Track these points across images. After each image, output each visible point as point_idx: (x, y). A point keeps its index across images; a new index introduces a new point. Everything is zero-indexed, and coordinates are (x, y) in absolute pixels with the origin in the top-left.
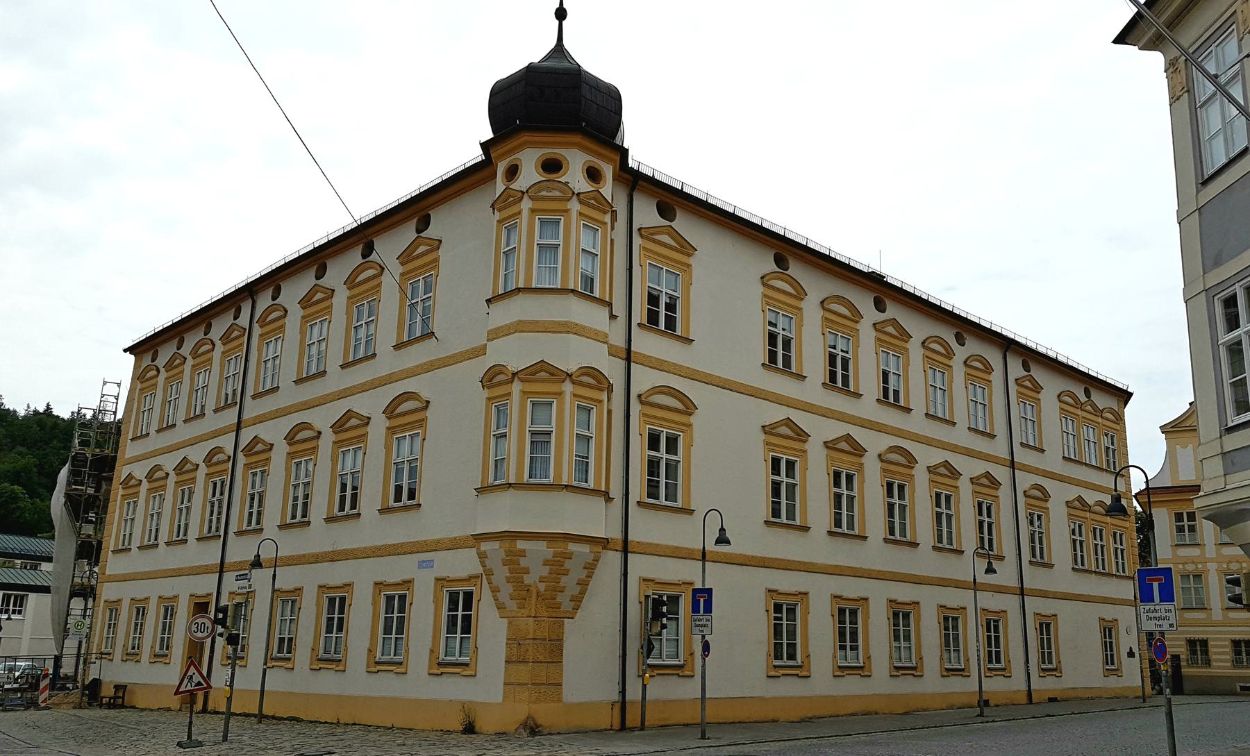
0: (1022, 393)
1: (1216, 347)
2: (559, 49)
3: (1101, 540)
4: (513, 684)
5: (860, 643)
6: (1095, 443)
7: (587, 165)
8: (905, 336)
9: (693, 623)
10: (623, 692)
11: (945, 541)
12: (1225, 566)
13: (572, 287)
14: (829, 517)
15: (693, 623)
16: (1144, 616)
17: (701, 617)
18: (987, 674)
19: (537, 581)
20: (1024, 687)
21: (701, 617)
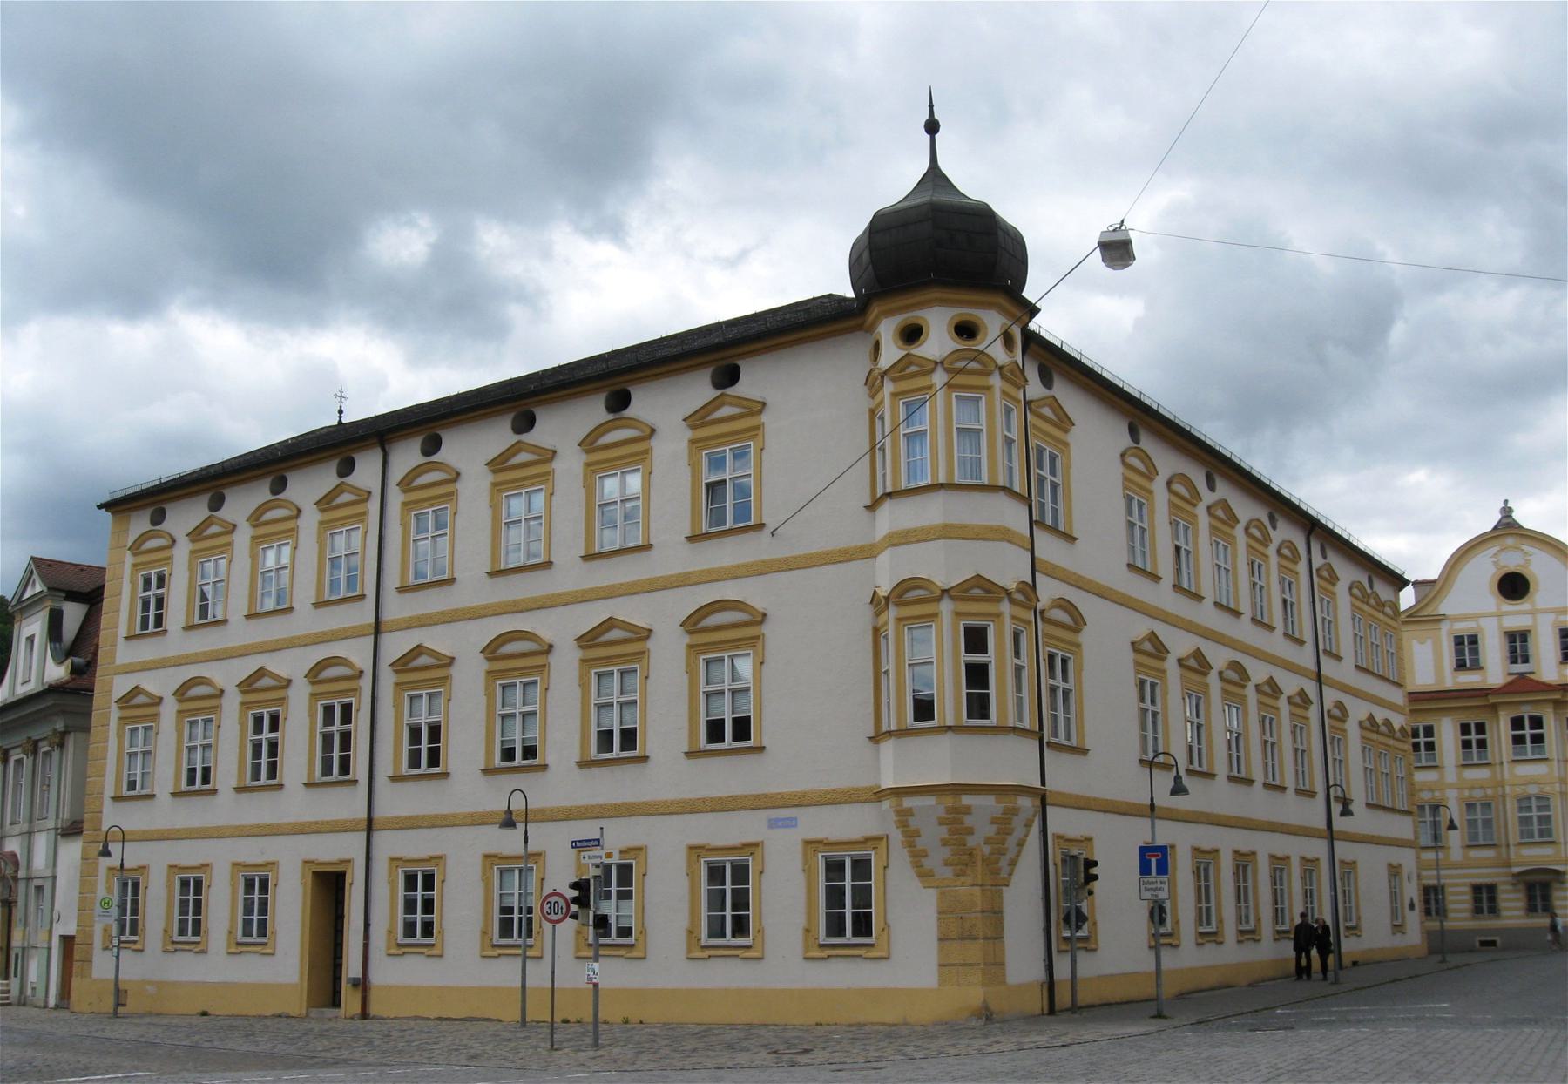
0: (1253, 548)
2: (934, 176)
3: (1065, 679)
4: (953, 965)
5: (497, 916)
6: (1227, 570)
7: (957, 320)
8: (1232, 519)
9: (1143, 887)
11: (1271, 778)
12: (1466, 793)
13: (1001, 484)
15: (1143, 887)
17: (1154, 880)
21: (1154, 880)
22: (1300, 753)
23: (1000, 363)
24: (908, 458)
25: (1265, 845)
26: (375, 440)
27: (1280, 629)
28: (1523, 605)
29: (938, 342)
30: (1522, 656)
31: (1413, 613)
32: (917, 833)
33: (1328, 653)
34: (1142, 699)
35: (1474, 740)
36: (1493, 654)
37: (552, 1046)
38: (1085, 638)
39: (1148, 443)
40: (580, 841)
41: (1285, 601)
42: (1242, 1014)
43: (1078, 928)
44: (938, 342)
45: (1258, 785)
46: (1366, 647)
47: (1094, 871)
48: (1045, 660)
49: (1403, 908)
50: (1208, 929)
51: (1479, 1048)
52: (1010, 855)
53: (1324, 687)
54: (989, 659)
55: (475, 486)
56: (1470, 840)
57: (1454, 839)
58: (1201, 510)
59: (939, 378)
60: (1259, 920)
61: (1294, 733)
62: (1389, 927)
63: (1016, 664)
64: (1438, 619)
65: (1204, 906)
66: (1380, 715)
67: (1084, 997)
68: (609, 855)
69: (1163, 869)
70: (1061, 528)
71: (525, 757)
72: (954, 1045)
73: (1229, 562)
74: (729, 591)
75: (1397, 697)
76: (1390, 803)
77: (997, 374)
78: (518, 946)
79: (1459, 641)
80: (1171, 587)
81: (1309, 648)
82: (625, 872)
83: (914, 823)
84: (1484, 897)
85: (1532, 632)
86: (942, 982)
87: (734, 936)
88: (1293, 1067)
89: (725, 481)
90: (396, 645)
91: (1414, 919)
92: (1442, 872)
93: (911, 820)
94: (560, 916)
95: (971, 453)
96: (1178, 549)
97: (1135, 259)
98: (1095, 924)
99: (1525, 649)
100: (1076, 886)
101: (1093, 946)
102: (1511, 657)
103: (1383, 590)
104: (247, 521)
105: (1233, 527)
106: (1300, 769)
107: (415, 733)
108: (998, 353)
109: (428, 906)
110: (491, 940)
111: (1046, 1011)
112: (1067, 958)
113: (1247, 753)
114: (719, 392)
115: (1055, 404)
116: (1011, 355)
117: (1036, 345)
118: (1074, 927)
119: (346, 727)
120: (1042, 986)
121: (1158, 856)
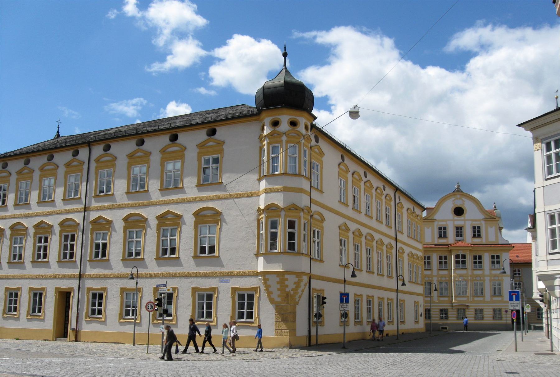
1: (547, 229)
3: (318, 238)
7: (290, 120)
8: (372, 187)
10: (309, 331)
14: (8, 200)
15: (341, 307)
17: (344, 304)
18: (313, 325)
19: (291, 290)
20: (396, 329)
21: (344, 304)
22: (389, 265)
24: (272, 164)
25: (377, 294)
26: (87, 145)
27: (385, 223)
28: (462, 218)
29: (284, 126)
30: (460, 234)
31: (425, 219)
32: (270, 286)
33: (399, 231)
34: (367, 254)
35: (443, 261)
36: (451, 233)
37: (148, 352)
38: (325, 224)
39: (347, 161)
40: (159, 285)
41: (386, 214)
43: (319, 319)
44: (284, 126)
46: (416, 233)
47: (325, 301)
49: (418, 316)
50: (358, 321)
51: (446, 360)
52: (299, 294)
54: (295, 231)
55: (122, 162)
56: (440, 294)
57: (435, 294)
58: (362, 184)
59: (284, 138)
60: (393, 319)
61: (387, 257)
62: (414, 322)
64: (433, 221)
65: (357, 313)
66: (414, 252)
67: (320, 342)
68: (169, 290)
69: (347, 301)
70: (345, 203)
71: (136, 256)
72: (281, 355)
73: (380, 207)
74: (210, 204)
75: (420, 246)
76: (421, 282)
78: (133, 319)
79: (440, 228)
80: (364, 215)
81: (393, 229)
82: (170, 296)
83: (269, 283)
84: (444, 313)
85: (464, 227)
87: (206, 318)
88: (392, 363)
90: (93, 216)
91: (422, 320)
92: (432, 304)
93: (268, 282)
94: (152, 309)
95: (293, 164)
96: (354, 196)
97: (359, 116)
98: (324, 317)
99: (461, 232)
101: (323, 325)
102: (457, 235)
103: (418, 211)
104: (38, 169)
105: (360, 182)
106: (389, 269)
107: (98, 246)
108: (304, 131)
109: (100, 304)
110: (122, 316)
111: (308, 345)
113: (383, 267)
114: (209, 137)
115: (320, 149)
117: (313, 127)
119: (72, 243)
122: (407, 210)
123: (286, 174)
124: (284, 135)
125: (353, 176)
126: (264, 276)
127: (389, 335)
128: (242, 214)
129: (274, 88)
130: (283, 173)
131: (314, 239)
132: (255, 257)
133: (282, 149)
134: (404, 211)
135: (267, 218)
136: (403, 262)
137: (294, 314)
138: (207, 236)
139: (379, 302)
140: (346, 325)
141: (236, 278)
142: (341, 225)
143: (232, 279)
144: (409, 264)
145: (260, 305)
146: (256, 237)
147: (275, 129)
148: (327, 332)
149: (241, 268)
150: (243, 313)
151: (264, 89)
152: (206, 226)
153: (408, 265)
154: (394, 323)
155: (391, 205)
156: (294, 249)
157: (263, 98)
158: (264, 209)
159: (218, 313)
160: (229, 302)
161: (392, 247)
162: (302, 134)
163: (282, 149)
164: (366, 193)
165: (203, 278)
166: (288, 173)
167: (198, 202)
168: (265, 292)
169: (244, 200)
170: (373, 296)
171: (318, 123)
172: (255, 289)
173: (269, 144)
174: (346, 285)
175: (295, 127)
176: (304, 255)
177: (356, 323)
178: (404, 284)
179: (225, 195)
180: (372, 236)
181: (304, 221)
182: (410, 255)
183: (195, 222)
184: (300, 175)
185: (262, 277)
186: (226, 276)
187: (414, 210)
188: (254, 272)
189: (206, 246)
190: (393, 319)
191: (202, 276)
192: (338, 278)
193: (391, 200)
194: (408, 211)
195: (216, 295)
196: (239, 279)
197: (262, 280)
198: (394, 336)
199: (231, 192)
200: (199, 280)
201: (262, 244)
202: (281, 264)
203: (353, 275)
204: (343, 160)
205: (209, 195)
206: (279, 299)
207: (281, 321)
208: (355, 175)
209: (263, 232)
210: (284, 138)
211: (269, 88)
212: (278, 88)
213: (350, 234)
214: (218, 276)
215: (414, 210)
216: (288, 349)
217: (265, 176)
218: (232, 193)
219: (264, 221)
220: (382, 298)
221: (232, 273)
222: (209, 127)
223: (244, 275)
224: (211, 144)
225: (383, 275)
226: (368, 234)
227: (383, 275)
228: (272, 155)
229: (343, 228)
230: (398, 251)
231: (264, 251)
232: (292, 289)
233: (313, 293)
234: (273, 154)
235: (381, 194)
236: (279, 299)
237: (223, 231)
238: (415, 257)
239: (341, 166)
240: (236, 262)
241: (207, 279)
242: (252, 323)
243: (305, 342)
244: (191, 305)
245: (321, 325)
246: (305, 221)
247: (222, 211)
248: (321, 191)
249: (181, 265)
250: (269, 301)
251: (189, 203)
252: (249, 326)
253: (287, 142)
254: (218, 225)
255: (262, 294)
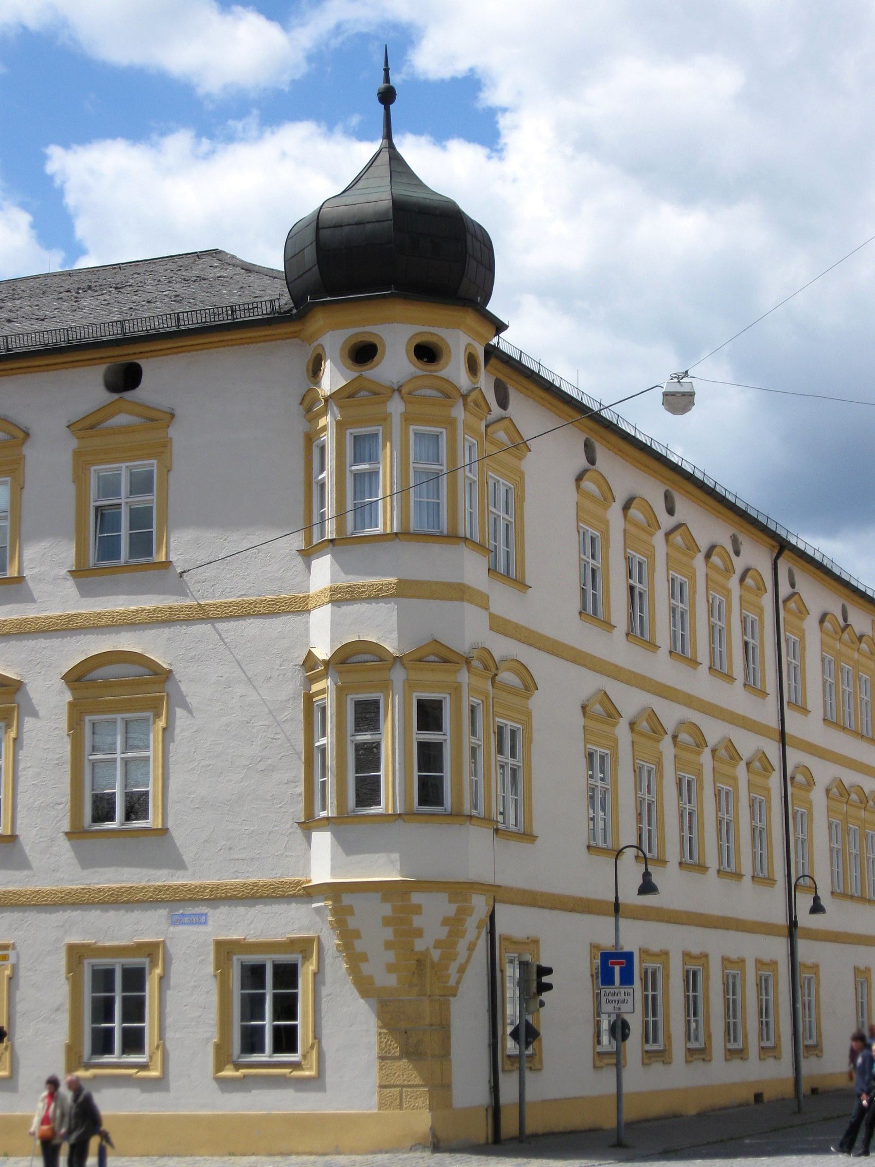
3: (513, 755)
8: (692, 546)
10: (495, 1089)
16: (604, 999)
17: (617, 991)
21: (617, 991)
22: (759, 835)
23: (464, 391)
24: (355, 500)
32: (357, 934)
38: (537, 703)
39: (607, 462)
41: (746, 644)
42: (708, 1143)
43: (528, 1044)
45: (712, 872)
47: (545, 979)
48: (495, 733)
52: (461, 959)
53: (788, 748)
54: (443, 737)
58: (659, 539)
59: (396, 407)
60: (779, 1037)
61: (752, 806)
63: (472, 747)
67: (531, 1127)
77: (460, 402)
81: (772, 700)
83: (353, 923)
86: (381, 1106)
89: (120, 504)
97: (694, 405)
100: (526, 997)
110: (80, 1057)
111: (490, 1140)
112: (515, 1076)
114: (115, 396)
116: (474, 380)
117: (492, 353)
118: (620, 1039)
120: (487, 1110)
121: (623, 963)
122: (822, 621)
123: (404, 535)
124: (396, 396)
125: (625, 516)
126: (336, 899)
127: (766, 1097)
128: (249, 679)
129: (357, 224)
130: (395, 531)
131: (500, 758)
132: (299, 831)
133: (388, 444)
134: (811, 624)
135: (341, 692)
136: (811, 820)
137: (444, 1028)
138: (119, 756)
139: (728, 976)
140: (531, 1069)
141: (230, 906)
142: (588, 700)
143: (218, 911)
144: (830, 827)
145: (324, 1000)
146: (300, 758)
147: (363, 373)
148: (553, 1093)
149: (248, 872)
150: (110, 1032)
151: (318, 229)
152: (114, 722)
153: (826, 831)
154: (780, 1052)
155: (761, 609)
156: (439, 802)
157: (316, 262)
158: (329, 661)
159: (169, 1034)
160: (208, 992)
161: (767, 768)
162: (457, 389)
163: (388, 444)
164: (671, 572)
165: (107, 911)
166: (412, 530)
167: (79, 635)
168: (338, 954)
169: (252, 627)
170: (706, 956)
171: (508, 341)
172: (304, 946)
173: (341, 426)
174: (622, 922)
175: (431, 367)
176: (474, 821)
177: (649, 1057)
178: (817, 908)
179: (180, 609)
180: (696, 730)
181: (471, 699)
182: (835, 790)
183: (72, 706)
184: (453, 537)
185: (330, 903)
186: (195, 900)
187: (845, 620)
188: (298, 883)
189: (114, 793)
190: (778, 1036)
191: (104, 903)
192: (584, 896)
193: (760, 588)
194: (827, 624)
195: (158, 971)
196: (241, 910)
197: (328, 912)
198: (781, 1101)
199: (204, 598)
200: (94, 916)
201: (324, 783)
202: (396, 856)
203: (647, 887)
204: (592, 460)
205: (121, 609)
206: (391, 981)
207: (399, 1058)
208: (633, 512)
209: (327, 741)
210: (396, 407)
211: (338, 226)
212: (369, 227)
213: (622, 731)
214: (162, 901)
215: (845, 620)
216: (427, 1154)
217: (332, 541)
218: (207, 602)
219: (330, 701)
220: (736, 962)
221: (215, 888)
222: (112, 360)
223: (261, 897)
224: (122, 419)
225: (738, 876)
226: (682, 723)
227: (738, 876)
228: (354, 468)
229: (598, 708)
230: (792, 778)
231: (335, 811)
232: (438, 944)
233: (503, 951)
234: (355, 462)
235: (727, 570)
236: (391, 981)
237: (178, 738)
238: (854, 796)
239: (588, 485)
240: (230, 849)
241: (122, 912)
242: (296, 1066)
243: (482, 1131)
244: (67, 1006)
245: (704, 1060)
246: (475, 700)
247: (170, 664)
248: (521, 585)
249: (23, 864)
250: (352, 986)
251: (45, 639)
252: (283, 1076)
253: (408, 419)
254: (158, 715)
255: (328, 961)
